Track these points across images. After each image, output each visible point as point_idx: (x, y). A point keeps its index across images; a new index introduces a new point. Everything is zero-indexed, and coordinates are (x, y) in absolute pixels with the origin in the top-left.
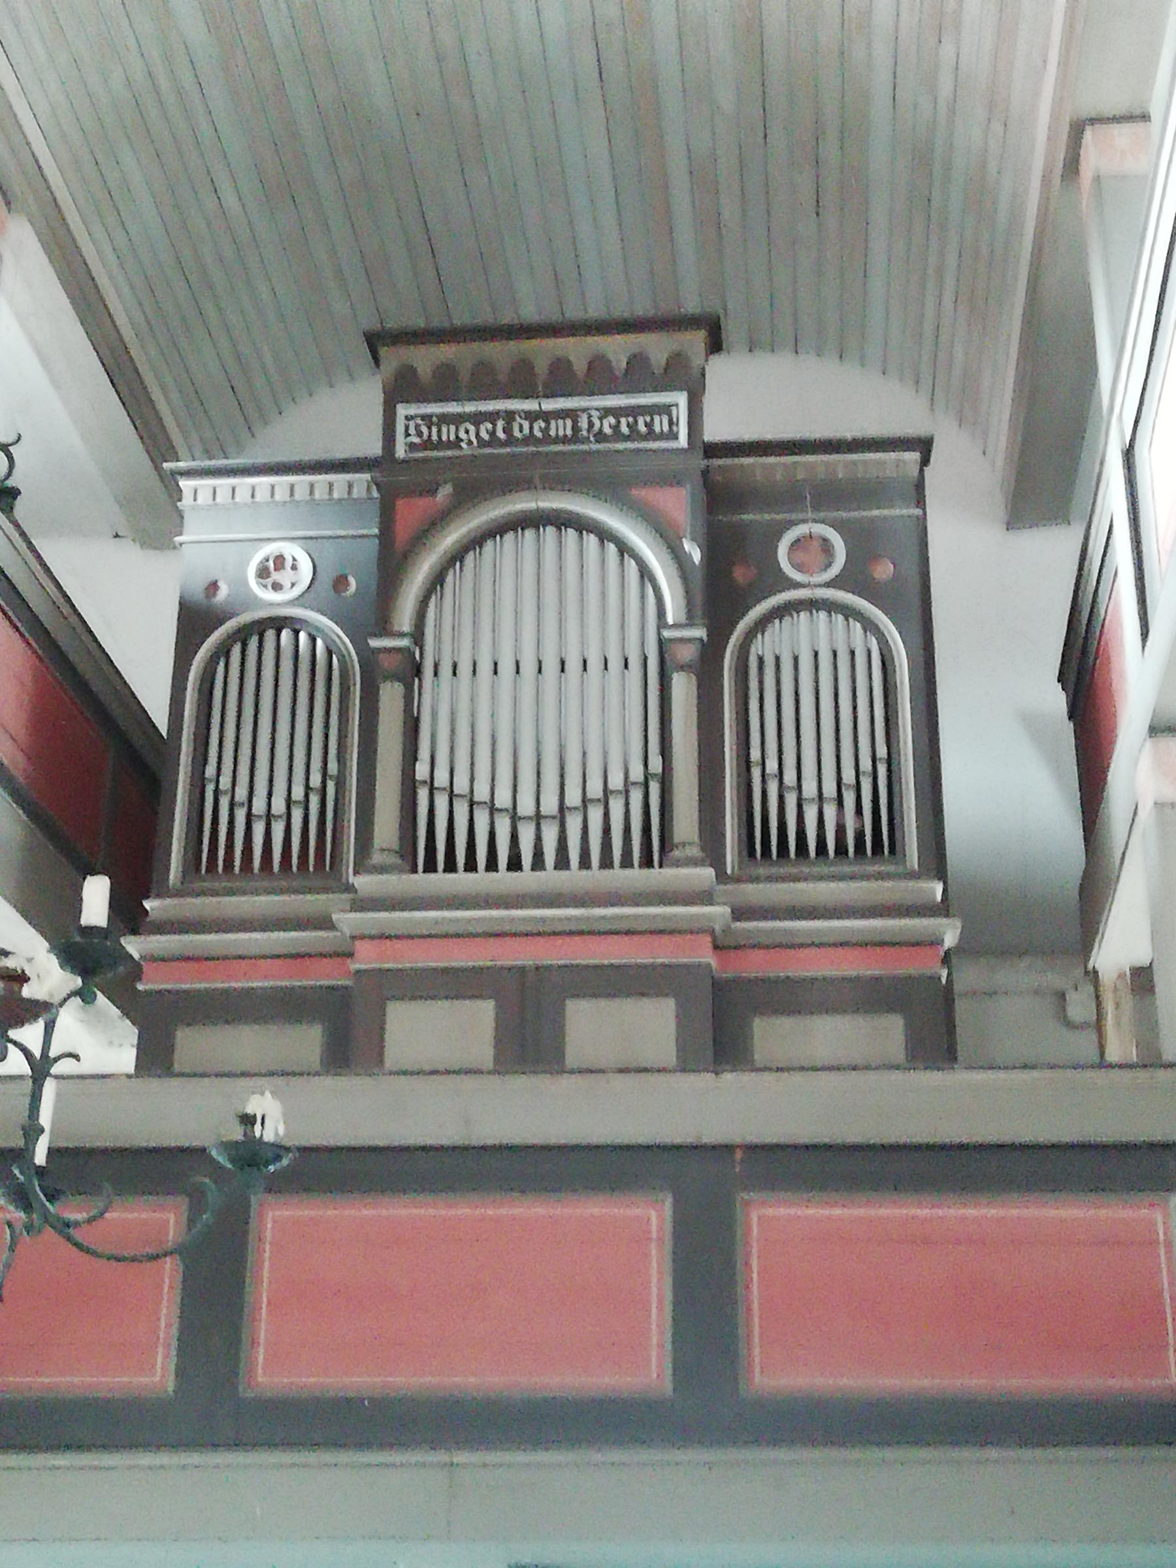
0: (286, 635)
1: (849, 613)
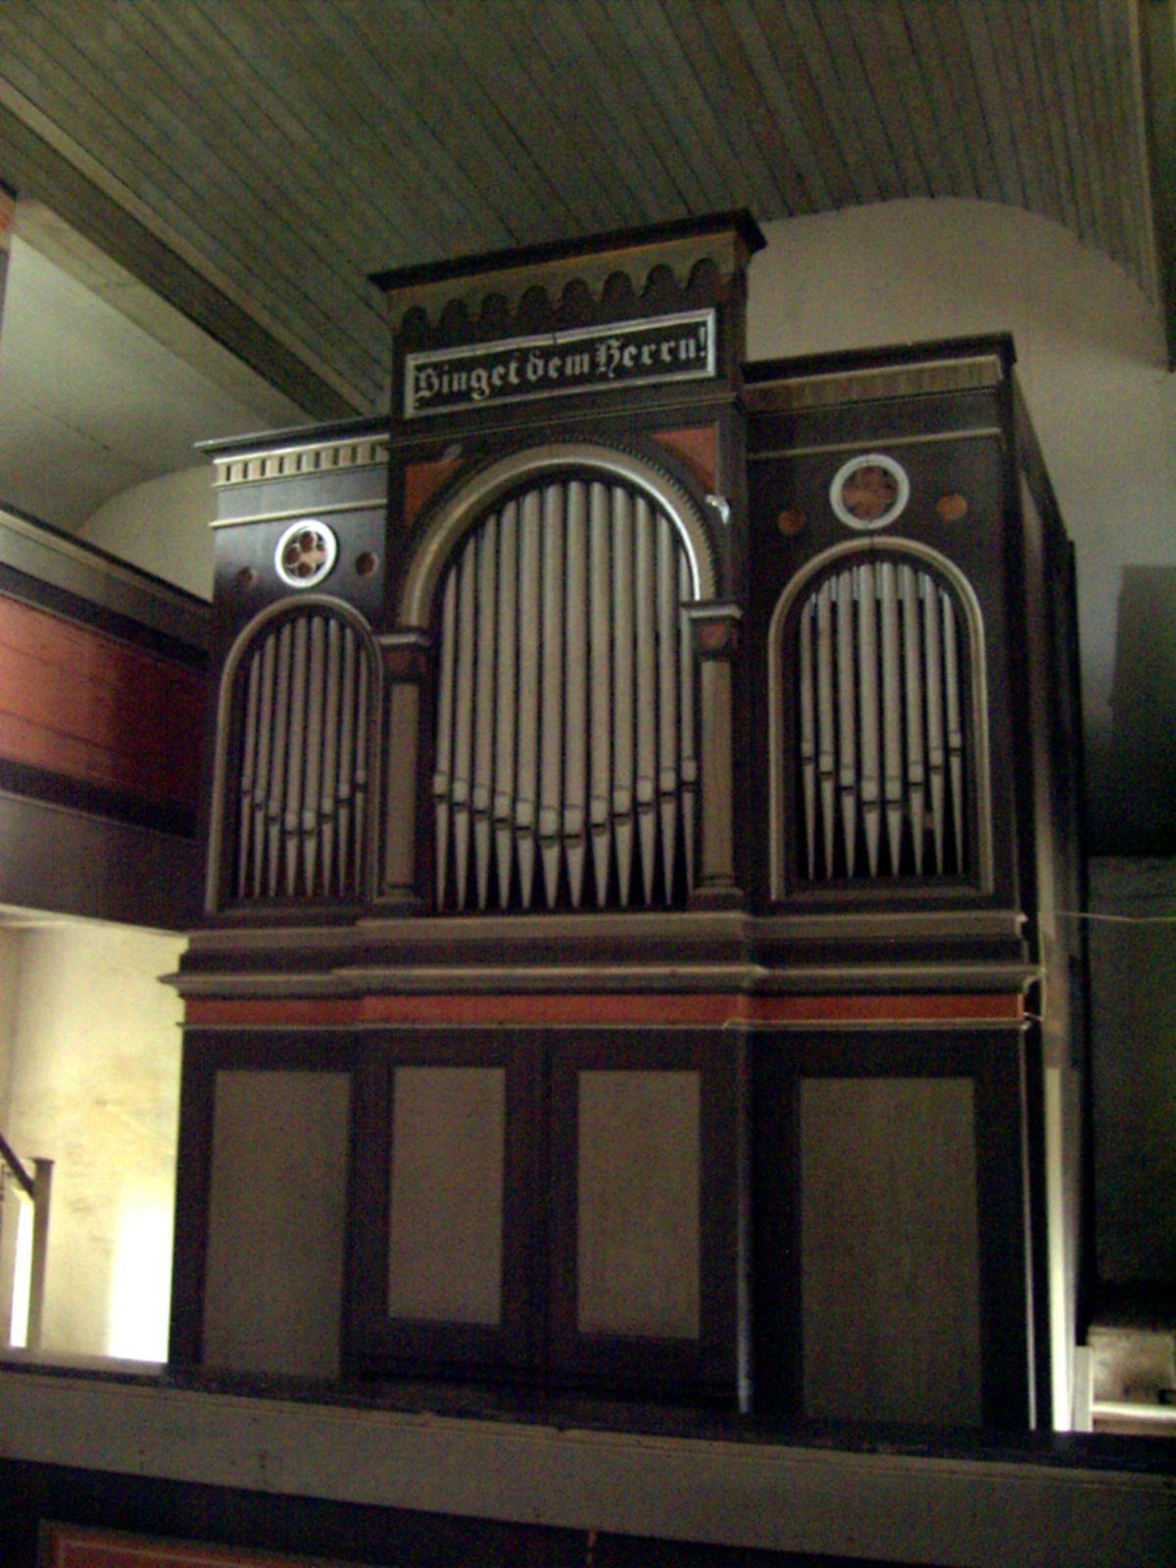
0: (317, 622)
1: (918, 564)
